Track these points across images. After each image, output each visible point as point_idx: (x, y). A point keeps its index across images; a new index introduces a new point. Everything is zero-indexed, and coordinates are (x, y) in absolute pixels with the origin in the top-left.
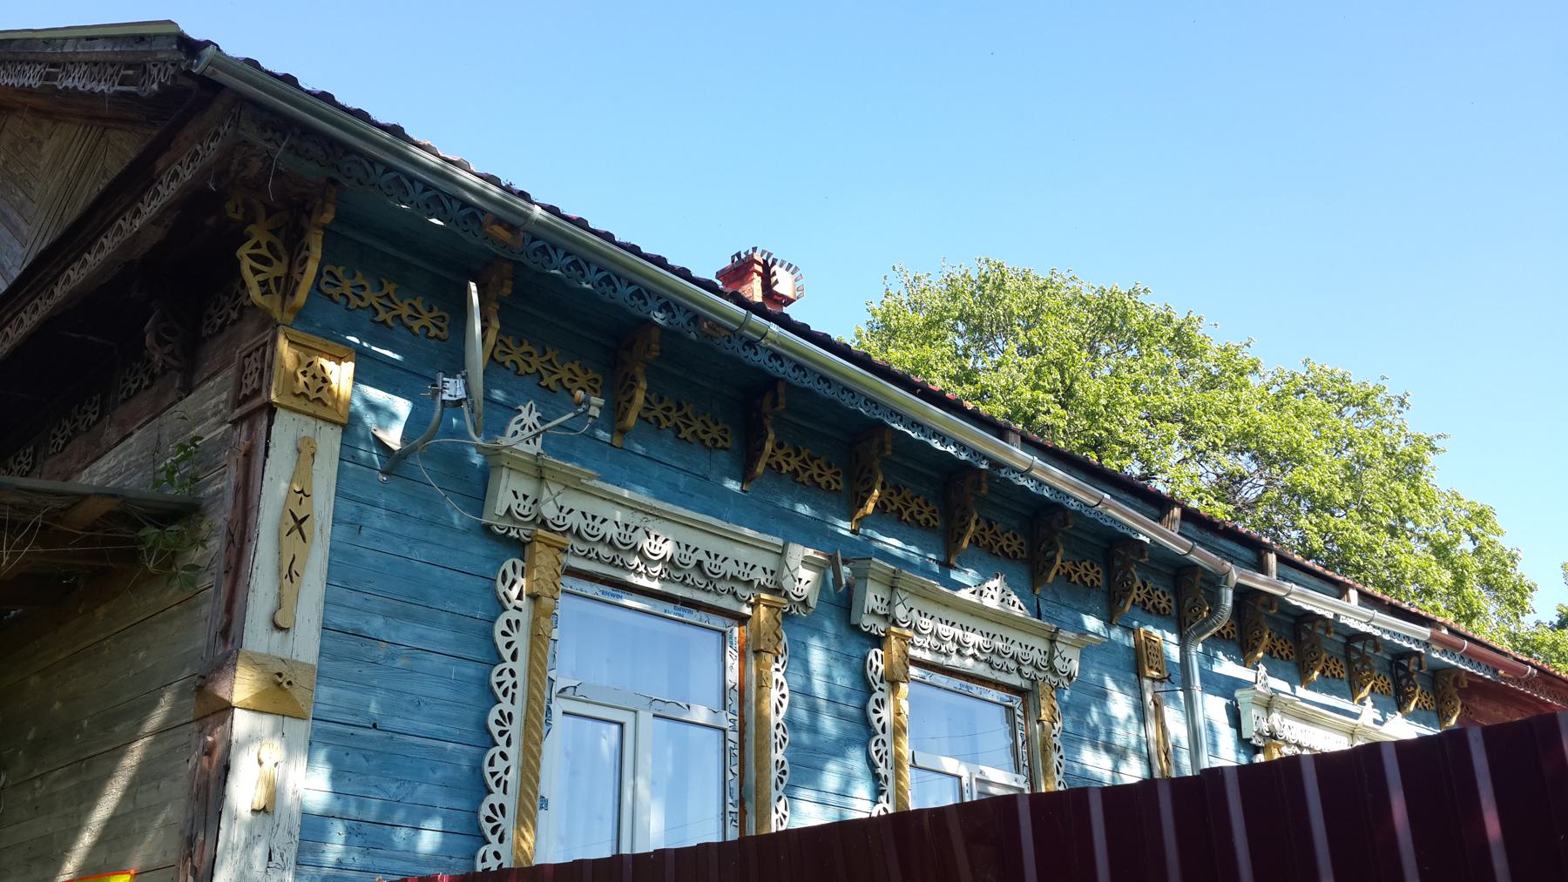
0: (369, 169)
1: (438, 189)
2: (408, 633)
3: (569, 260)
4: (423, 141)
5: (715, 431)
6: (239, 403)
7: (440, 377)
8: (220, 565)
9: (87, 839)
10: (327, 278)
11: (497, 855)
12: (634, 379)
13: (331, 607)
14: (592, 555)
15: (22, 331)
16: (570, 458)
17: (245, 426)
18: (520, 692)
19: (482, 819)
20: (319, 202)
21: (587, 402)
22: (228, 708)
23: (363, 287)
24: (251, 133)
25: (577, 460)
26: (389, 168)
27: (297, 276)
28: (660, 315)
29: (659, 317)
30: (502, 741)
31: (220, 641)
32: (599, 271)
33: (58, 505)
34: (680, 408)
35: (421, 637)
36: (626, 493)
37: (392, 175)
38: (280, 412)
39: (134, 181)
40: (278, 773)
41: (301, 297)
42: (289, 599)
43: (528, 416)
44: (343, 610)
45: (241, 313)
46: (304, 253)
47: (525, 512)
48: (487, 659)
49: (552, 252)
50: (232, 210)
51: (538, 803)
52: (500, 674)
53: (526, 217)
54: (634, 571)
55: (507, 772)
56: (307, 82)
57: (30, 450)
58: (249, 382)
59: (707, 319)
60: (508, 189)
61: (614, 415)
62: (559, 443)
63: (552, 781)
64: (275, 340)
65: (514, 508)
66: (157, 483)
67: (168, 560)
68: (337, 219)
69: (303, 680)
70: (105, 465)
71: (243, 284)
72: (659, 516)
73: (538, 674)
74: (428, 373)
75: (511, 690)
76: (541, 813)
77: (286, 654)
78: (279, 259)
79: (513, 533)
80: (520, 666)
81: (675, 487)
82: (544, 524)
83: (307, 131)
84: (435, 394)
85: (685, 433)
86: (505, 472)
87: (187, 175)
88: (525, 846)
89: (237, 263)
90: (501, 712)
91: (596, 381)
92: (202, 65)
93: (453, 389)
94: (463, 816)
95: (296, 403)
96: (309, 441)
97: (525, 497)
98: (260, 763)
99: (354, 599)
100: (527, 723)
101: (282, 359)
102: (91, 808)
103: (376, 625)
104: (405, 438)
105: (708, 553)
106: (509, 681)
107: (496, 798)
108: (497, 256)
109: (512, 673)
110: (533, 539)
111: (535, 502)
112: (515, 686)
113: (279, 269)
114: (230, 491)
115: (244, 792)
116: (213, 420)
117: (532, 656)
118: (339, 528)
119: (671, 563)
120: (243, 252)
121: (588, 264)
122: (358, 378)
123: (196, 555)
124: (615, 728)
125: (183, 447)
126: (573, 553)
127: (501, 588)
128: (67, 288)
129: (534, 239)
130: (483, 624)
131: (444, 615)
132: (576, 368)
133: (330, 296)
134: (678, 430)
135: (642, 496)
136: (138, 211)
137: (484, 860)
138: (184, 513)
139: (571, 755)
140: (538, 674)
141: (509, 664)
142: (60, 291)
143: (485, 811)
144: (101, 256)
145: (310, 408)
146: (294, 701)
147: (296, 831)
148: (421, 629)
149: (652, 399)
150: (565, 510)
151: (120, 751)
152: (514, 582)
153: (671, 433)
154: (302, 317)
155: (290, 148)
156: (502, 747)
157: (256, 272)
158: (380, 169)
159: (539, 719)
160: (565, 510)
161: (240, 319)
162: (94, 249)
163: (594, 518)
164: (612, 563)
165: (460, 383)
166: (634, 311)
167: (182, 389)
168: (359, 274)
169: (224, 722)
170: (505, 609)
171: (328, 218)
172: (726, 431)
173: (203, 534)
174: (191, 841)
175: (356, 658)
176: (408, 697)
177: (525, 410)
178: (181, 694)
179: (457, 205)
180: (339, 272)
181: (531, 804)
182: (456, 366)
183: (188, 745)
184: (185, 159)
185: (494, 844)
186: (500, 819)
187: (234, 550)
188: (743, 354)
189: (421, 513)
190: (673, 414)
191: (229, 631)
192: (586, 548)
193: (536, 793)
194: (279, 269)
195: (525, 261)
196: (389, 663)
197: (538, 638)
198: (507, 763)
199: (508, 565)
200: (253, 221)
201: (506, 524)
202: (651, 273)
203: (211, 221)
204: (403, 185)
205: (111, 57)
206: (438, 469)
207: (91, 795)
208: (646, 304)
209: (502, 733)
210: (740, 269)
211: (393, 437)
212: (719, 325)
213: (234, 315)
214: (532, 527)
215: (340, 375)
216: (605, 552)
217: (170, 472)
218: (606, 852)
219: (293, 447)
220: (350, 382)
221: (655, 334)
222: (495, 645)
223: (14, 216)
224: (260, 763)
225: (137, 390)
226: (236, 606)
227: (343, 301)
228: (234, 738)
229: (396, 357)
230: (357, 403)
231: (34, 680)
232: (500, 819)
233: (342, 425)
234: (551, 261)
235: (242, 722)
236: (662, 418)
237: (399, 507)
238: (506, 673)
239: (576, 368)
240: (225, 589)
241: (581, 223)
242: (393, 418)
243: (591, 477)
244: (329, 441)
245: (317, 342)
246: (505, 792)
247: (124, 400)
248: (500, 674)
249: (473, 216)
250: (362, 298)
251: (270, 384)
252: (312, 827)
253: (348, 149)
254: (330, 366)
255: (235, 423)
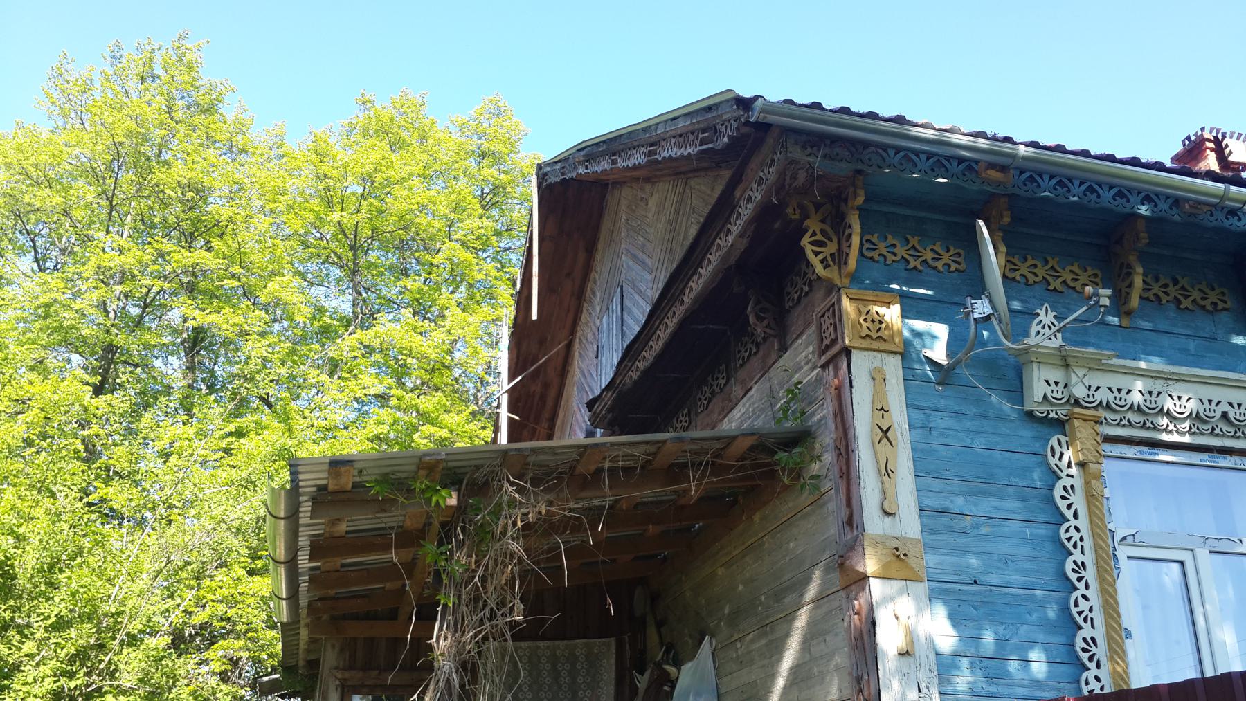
0: (884, 155)
1: (940, 155)
2: (986, 506)
3: (1054, 181)
4: (921, 121)
5: (1213, 297)
6: (823, 352)
7: (969, 301)
8: (834, 473)
9: (780, 683)
10: (867, 245)
11: (1097, 679)
12: (1129, 266)
13: (922, 493)
14: (1125, 422)
15: (668, 331)
16: (1085, 344)
17: (831, 368)
18: (1087, 543)
19: (1079, 650)
20: (851, 189)
21: (1096, 295)
22: (864, 578)
23: (894, 245)
24: (796, 153)
25: (1093, 345)
26: (898, 150)
27: (845, 249)
28: (1144, 208)
29: (1144, 210)
30: (1081, 585)
31: (847, 529)
32: (1081, 183)
33: (719, 447)
34: (1176, 282)
35: (996, 508)
36: (1143, 365)
37: (902, 154)
38: (854, 351)
39: (723, 209)
40: (911, 622)
41: (852, 264)
42: (891, 494)
43: (1046, 316)
44: (931, 494)
45: (810, 286)
46: (848, 231)
47: (1059, 396)
48: (1053, 520)
49: (1070, 185)
50: (792, 214)
51: (1123, 634)
52: (1067, 531)
53: (1014, 156)
54: (1165, 430)
55: (1091, 610)
56: (798, 101)
57: (686, 412)
58: (827, 334)
59: (1187, 200)
60: (994, 138)
61: (1120, 303)
62: (1074, 335)
63: (1130, 615)
64: (839, 300)
65: (1049, 394)
66: (779, 421)
67: (797, 474)
68: (866, 201)
69: (915, 551)
70: (737, 413)
71: (808, 264)
72: (1178, 379)
73: (1099, 527)
74: (956, 299)
75: (1079, 544)
76: (1127, 642)
77: (898, 534)
78: (830, 239)
79: (1052, 415)
80: (1083, 522)
81: (1185, 351)
82: (1077, 403)
83: (835, 140)
84: (968, 314)
85: (1186, 303)
86: (1035, 366)
87: (757, 196)
88: (1119, 669)
89: (803, 250)
90: (1075, 562)
91: (959, 254)
92: (756, 115)
93: (981, 308)
94: (1063, 649)
95: (865, 344)
96: (879, 370)
97: (1057, 383)
98: (897, 618)
99: (936, 484)
100: (1099, 570)
101: (847, 313)
102: (779, 660)
103: (958, 503)
104: (950, 353)
105: (1230, 404)
106: (1076, 537)
107: (1087, 632)
108: (993, 195)
109: (1077, 529)
110: (1071, 417)
111: (1066, 386)
112: (1081, 539)
113: (832, 247)
114: (830, 418)
115: (889, 639)
116: (806, 368)
117: (1091, 513)
118: (915, 432)
119: (1196, 418)
120: (805, 241)
121: (1070, 180)
122: (905, 315)
123: (815, 468)
124: (1176, 567)
125: (789, 391)
126: (1107, 423)
127: (1053, 461)
128: (692, 296)
129: (1022, 173)
130: (1044, 492)
131: (1010, 489)
132: (1077, 270)
133: (872, 258)
134: (1178, 302)
135: (1158, 364)
136: (729, 230)
137: (1087, 683)
138: (800, 438)
139: (1143, 594)
140: (1099, 527)
141: (1073, 522)
142: (688, 299)
143: (1080, 644)
144: (710, 268)
145: (875, 345)
146: (912, 568)
147: (934, 668)
148: (995, 502)
149: (1149, 280)
150: (1093, 389)
151: (791, 617)
152: (1062, 455)
153: (1172, 306)
154: (855, 278)
155: (825, 156)
156: (1082, 590)
157: (816, 254)
158: (892, 152)
159: (1109, 565)
160: (1093, 389)
161: (811, 290)
162: (705, 264)
163: (1119, 390)
164: (1144, 426)
165: (986, 302)
166: (1120, 209)
167: (779, 350)
168: (890, 236)
169: (863, 589)
170: (1059, 478)
171: (860, 200)
172: (1223, 294)
173: (817, 451)
174: (859, 680)
175: (950, 531)
176: (996, 557)
177: (1042, 313)
178: (827, 570)
179: (955, 163)
180: (875, 239)
181: (1117, 636)
182: (979, 288)
183: (840, 608)
184: (754, 185)
185: (1093, 671)
186: (1094, 650)
187: (843, 460)
188: (1227, 223)
189: (974, 410)
190: (1172, 289)
191: (852, 520)
192: (1117, 417)
193: (1120, 626)
194: (832, 247)
195: (1016, 191)
196: (976, 531)
197: (1092, 498)
198: (1089, 600)
199: (1053, 441)
200: (807, 217)
201: (1045, 408)
202: (1130, 174)
203: (777, 225)
204: (911, 160)
205: (691, 128)
206: (989, 371)
207: (777, 649)
208: (1128, 201)
209: (1079, 579)
210: (1194, 149)
211: (939, 353)
212: (1200, 203)
213: (806, 289)
214: (1068, 407)
215: (892, 314)
216: (1135, 418)
217: (785, 410)
218: (1192, 674)
219: (868, 377)
220: (900, 319)
221: (1141, 225)
222: (1058, 508)
223: (640, 255)
224: (897, 618)
225: (749, 357)
226: (854, 502)
227: (881, 259)
228: (874, 600)
229: (929, 292)
230: (906, 334)
231: (720, 572)
232: (1094, 650)
233: (900, 353)
234: (1039, 186)
235: (877, 588)
236: (1161, 295)
237: (956, 409)
238: (1072, 529)
239: (1077, 270)
240: (843, 490)
241: (1060, 149)
242: (937, 340)
243: (1110, 357)
244: (893, 367)
245: (870, 295)
246: (1093, 627)
247: (742, 366)
248: (1067, 531)
249: (970, 168)
250: (895, 254)
251: (843, 333)
252: (945, 666)
253: (866, 144)
254: (882, 310)
255: (823, 367)
